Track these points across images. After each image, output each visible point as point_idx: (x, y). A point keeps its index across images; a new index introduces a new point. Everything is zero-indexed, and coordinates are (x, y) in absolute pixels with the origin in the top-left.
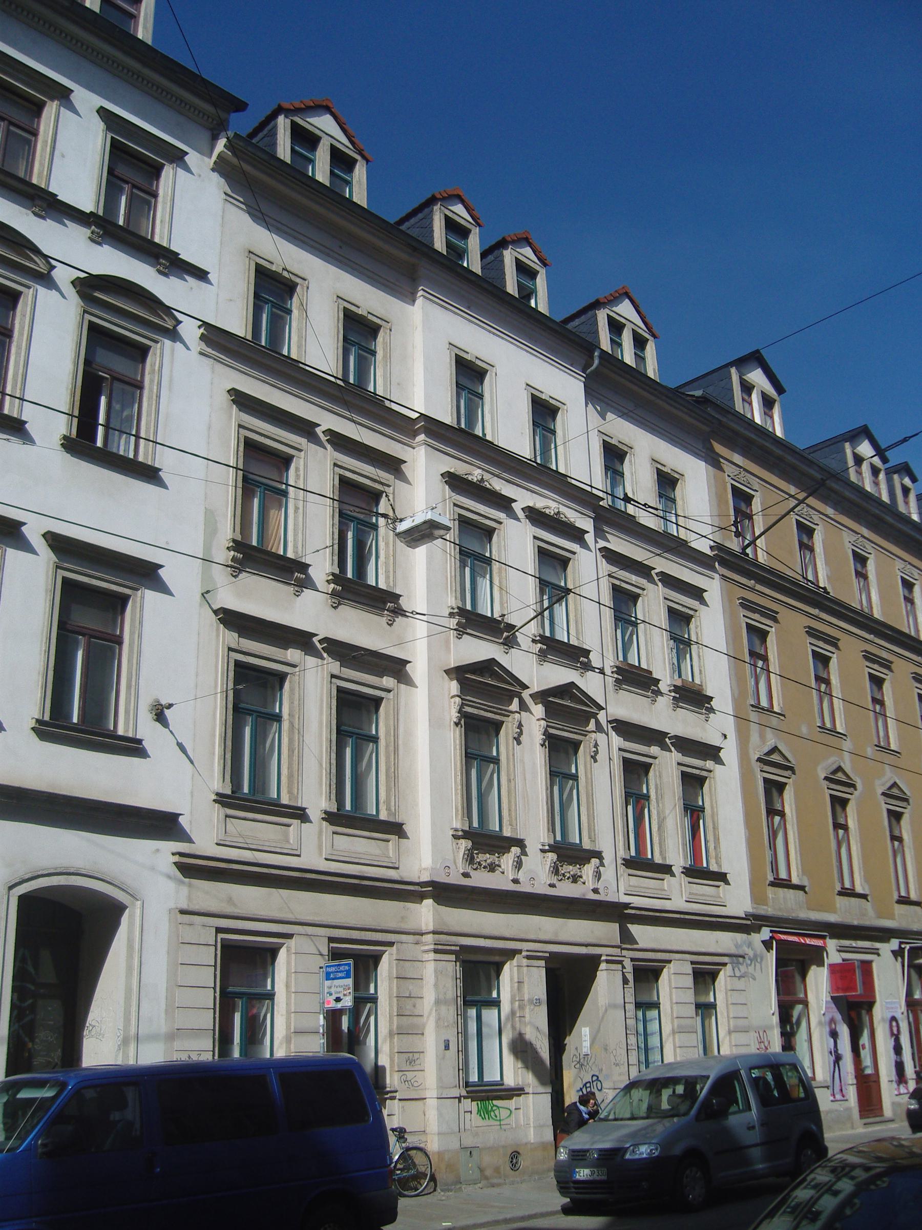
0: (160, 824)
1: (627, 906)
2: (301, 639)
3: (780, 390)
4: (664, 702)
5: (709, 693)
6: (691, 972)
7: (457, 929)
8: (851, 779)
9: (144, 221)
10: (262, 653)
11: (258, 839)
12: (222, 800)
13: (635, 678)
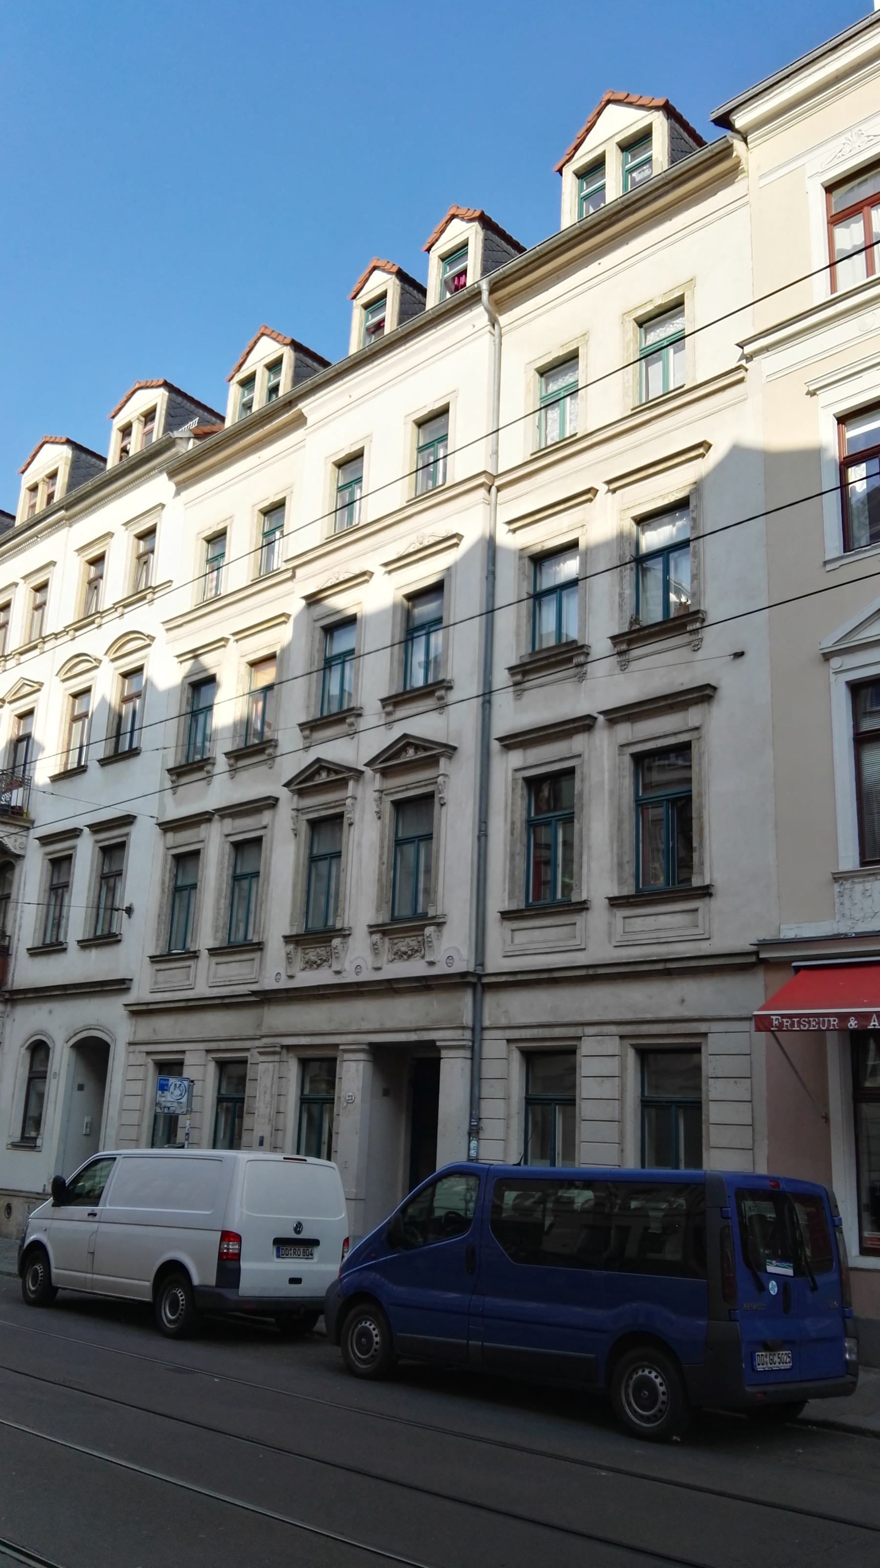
0: (120, 986)
7: (283, 1029)
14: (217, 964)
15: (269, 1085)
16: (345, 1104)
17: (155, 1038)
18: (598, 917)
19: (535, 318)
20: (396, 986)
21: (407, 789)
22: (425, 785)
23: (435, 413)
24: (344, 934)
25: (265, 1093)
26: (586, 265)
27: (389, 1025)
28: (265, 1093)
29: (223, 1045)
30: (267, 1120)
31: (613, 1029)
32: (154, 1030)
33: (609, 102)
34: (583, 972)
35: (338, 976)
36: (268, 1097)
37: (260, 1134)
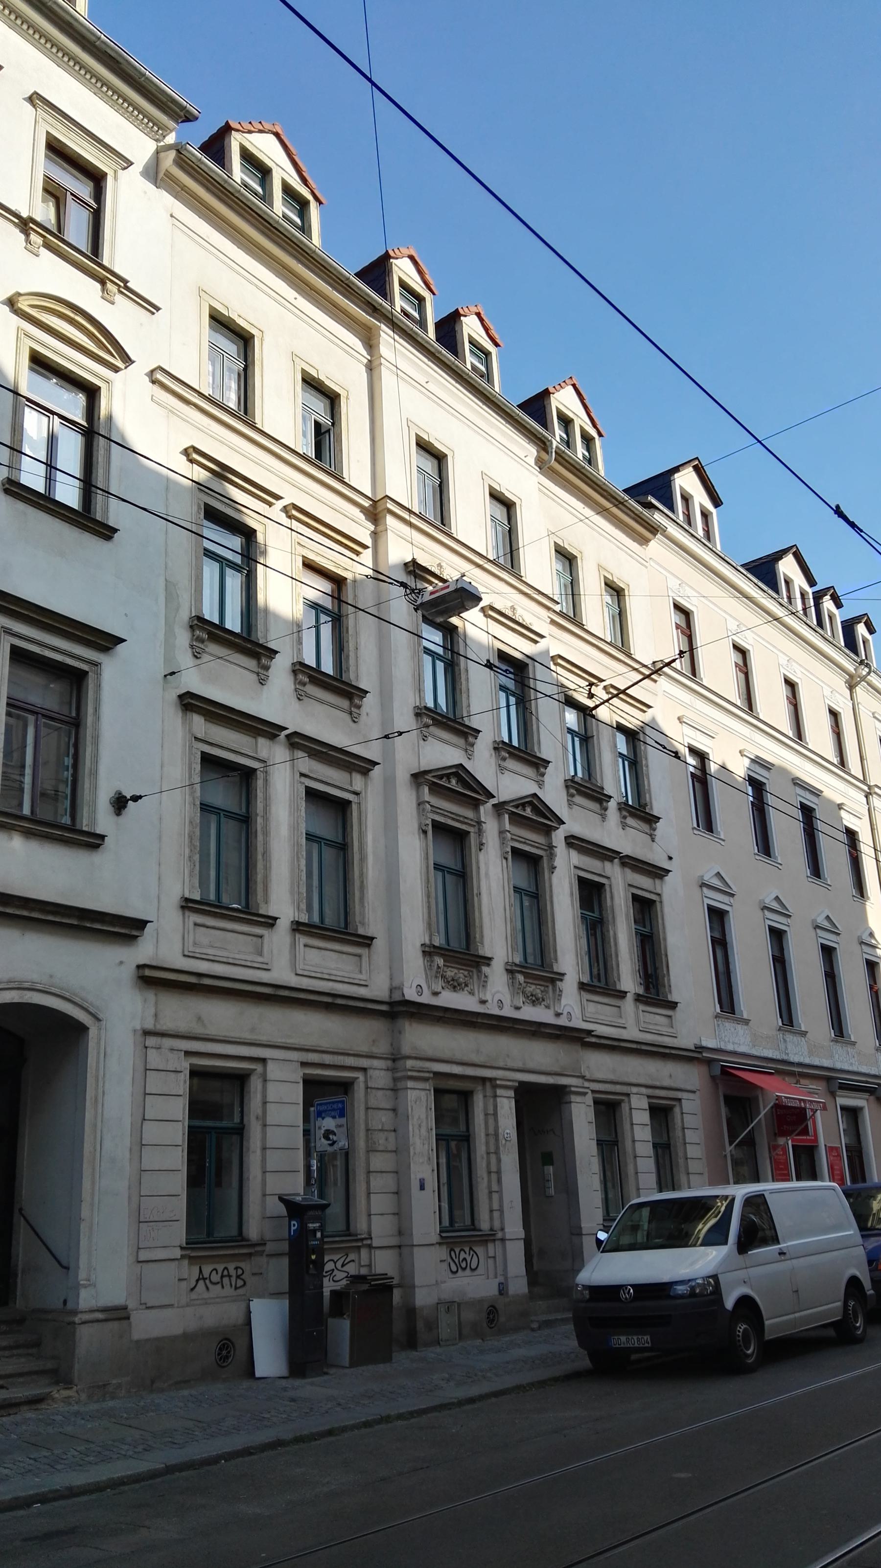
0: (125, 929)
1: (589, 1033)
2: (266, 729)
3: (717, 502)
4: (279, 939)
5: (655, 813)
6: (647, 1107)
7: (430, 1053)
8: (788, 910)
9: (845, 1127)
10: (231, 743)
11: (225, 950)
12: (187, 905)
13: (588, 789)
14: (305, 946)
15: (423, 1116)
16: (504, 1142)
17: (199, 1030)
18: (279, 939)
19: (562, 506)
20: (543, 1030)
21: (525, 843)
22: (537, 847)
23: (503, 498)
24: (488, 961)
25: (420, 1126)
26: (579, 499)
27: (531, 1065)
28: (420, 1126)
29: (327, 1059)
30: (426, 1159)
31: (643, 1090)
32: (199, 1019)
33: (277, 135)
34: (634, 1046)
35: (483, 1006)
36: (424, 1131)
37: (420, 1176)
